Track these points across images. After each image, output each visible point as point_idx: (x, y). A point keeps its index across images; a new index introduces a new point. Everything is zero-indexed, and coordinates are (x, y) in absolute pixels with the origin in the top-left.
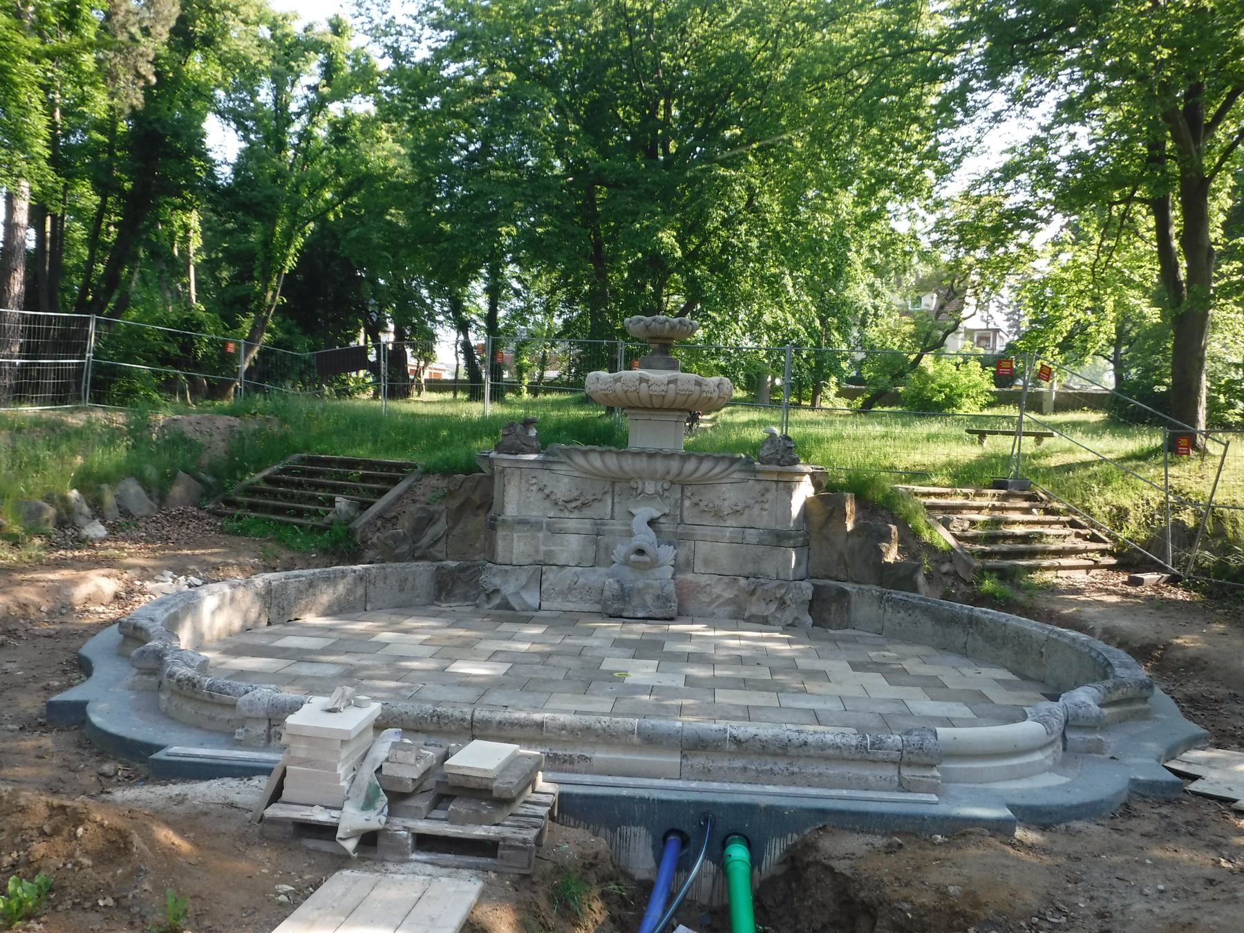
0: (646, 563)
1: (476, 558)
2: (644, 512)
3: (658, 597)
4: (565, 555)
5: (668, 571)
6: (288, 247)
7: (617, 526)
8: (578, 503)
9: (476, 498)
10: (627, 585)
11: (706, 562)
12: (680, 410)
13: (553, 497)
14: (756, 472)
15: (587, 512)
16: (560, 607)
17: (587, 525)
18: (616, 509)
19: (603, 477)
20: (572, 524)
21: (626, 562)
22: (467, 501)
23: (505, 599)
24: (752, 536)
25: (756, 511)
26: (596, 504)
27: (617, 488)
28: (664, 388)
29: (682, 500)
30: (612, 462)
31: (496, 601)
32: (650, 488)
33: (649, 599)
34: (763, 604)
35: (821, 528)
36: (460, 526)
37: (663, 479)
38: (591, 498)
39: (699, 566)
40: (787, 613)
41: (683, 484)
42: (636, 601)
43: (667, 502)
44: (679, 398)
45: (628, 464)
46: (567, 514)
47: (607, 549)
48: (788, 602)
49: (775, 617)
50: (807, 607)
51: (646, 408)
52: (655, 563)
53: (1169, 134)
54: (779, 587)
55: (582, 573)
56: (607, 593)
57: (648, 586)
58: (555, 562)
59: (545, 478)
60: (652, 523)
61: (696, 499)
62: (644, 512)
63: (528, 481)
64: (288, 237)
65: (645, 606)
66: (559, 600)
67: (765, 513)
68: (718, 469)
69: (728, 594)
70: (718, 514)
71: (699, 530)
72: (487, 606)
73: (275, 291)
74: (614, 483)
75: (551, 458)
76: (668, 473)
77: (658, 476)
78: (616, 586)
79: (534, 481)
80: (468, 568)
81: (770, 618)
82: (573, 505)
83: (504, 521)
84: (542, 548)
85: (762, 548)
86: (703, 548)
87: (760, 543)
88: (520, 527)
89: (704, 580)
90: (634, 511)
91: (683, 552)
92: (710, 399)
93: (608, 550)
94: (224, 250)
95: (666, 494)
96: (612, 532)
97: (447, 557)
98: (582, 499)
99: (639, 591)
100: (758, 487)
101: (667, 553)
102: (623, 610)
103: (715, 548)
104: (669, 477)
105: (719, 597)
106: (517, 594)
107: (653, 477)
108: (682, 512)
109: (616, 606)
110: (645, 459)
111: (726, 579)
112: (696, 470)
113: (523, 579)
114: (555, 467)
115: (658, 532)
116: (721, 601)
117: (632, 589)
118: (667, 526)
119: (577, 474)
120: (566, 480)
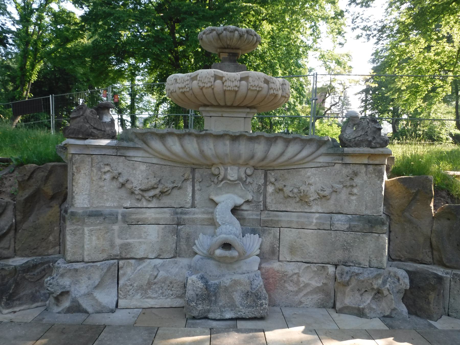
0: (232, 258)
1: (50, 251)
2: (227, 199)
3: (247, 295)
4: (144, 247)
5: (253, 263)
6: (32, 70)
7: (198, 214)
8: (157, 192)
9: (48, 189)
10: (212, 282)
11: (292, 250)
12: (248, 107)
13: (129, 186)
14: (344, 155)
15: (166, 201)
16: (139, 304)
17: (167, 214)
18: (197, 197)
19: (183, 164)
20: (150, 214)
21: (210, 256)
22: (38, 192)
23: (74, 301)
24: (340, 222)
25: (344, 195)
26: (176, 192)
27: (197, 175)
28: (237, 83)
29: (265, 185)
30: (192, 146)
31: (66, 304)
32: (233, 174)
33: (237, 297)
34: (357, 295)
35: (403, 211)
36: (31, 219)
37: (246, 164)
38: (171, 186)
39: (284, 254)
40: (384, 304)
41: (265, 169)
42: (223, 300)
43: (250, 188)
44: (250, 93)
45: (209, 147)
46: (145, 204)
47: (188, 239)
48: (386, 293)
49: (371, 309)
50: (402, 295)
51: (219, 106)
52: (242, 256)
53: (451, 6)
54: (377, 277)
55: (163, 265)
56: (190, 293)
57: (236, 283)
58: (132, 255)
59: (120, 165)
60: (235, 210)
61: (279, 185)
62: (227, 199)
63: (99, 169)
64: (33, 66)
65: (233, 306)
66: (138, 296)
67: (353, 198)
68: (304, 153)
69: (316, 283)
70: (303, 199)
71: (283, 217)
72: (56, 309)
73: (27, 91)
74: (193, 170)
75: (125, 144)
76: (252, 157)
77: (241, 162)
78: (200, 284)
79: (107, 168)
80: (35, 266)
81: (367, 311)
82: (152, 193)
83: (73, 214)
84: (118, 242)
85: (352, 235)
86: (289, 235)
87: (350, 229)
88: (92, 220)
89: (290, 268)
90: (216, 199)
91: (268, 240)
92: (276, 96)
93: (190, 240)
94: (9, 76)
95: (249, 180)
96: (193, 221)
97: (15, 254)
98: (160, 186)
99: (226, 288)
100: (346, 171)
101: (253, 243)
102: (209, 311)
103: (302, 235)
104: (252, 163)
105: (307, 285)
106: (89, 294)
107: (235, 162)
108: (265, 197)
109: (200, 307)
110: (228, 142)
111: (314, 268)
112: (282, 154)
113: (96, 278)
114: (131, 153)
115: (241, 219)
116: (308, 289)
117: (218, 286)
118: (250, 213)
119: (155, 161)
120: (143, 167)
